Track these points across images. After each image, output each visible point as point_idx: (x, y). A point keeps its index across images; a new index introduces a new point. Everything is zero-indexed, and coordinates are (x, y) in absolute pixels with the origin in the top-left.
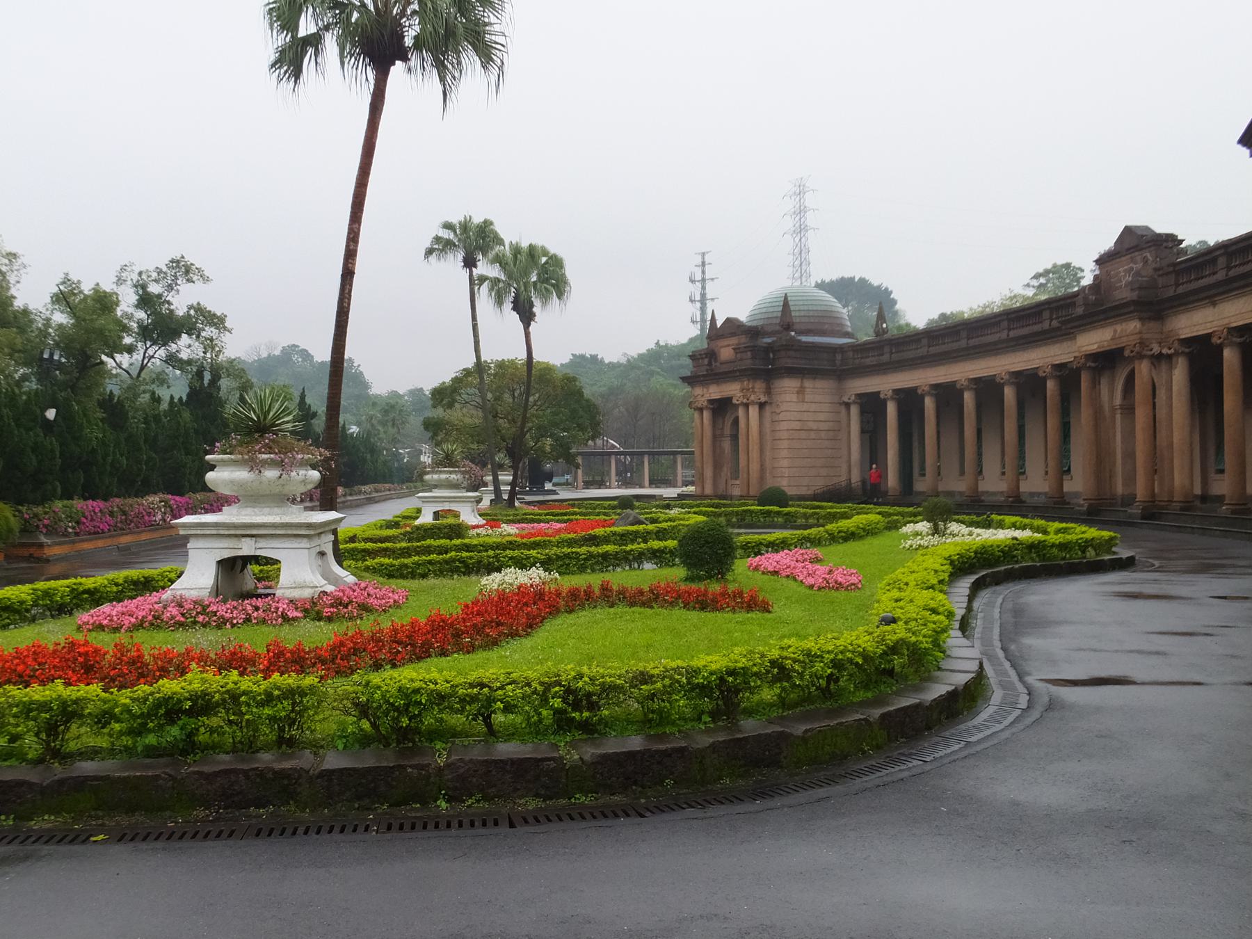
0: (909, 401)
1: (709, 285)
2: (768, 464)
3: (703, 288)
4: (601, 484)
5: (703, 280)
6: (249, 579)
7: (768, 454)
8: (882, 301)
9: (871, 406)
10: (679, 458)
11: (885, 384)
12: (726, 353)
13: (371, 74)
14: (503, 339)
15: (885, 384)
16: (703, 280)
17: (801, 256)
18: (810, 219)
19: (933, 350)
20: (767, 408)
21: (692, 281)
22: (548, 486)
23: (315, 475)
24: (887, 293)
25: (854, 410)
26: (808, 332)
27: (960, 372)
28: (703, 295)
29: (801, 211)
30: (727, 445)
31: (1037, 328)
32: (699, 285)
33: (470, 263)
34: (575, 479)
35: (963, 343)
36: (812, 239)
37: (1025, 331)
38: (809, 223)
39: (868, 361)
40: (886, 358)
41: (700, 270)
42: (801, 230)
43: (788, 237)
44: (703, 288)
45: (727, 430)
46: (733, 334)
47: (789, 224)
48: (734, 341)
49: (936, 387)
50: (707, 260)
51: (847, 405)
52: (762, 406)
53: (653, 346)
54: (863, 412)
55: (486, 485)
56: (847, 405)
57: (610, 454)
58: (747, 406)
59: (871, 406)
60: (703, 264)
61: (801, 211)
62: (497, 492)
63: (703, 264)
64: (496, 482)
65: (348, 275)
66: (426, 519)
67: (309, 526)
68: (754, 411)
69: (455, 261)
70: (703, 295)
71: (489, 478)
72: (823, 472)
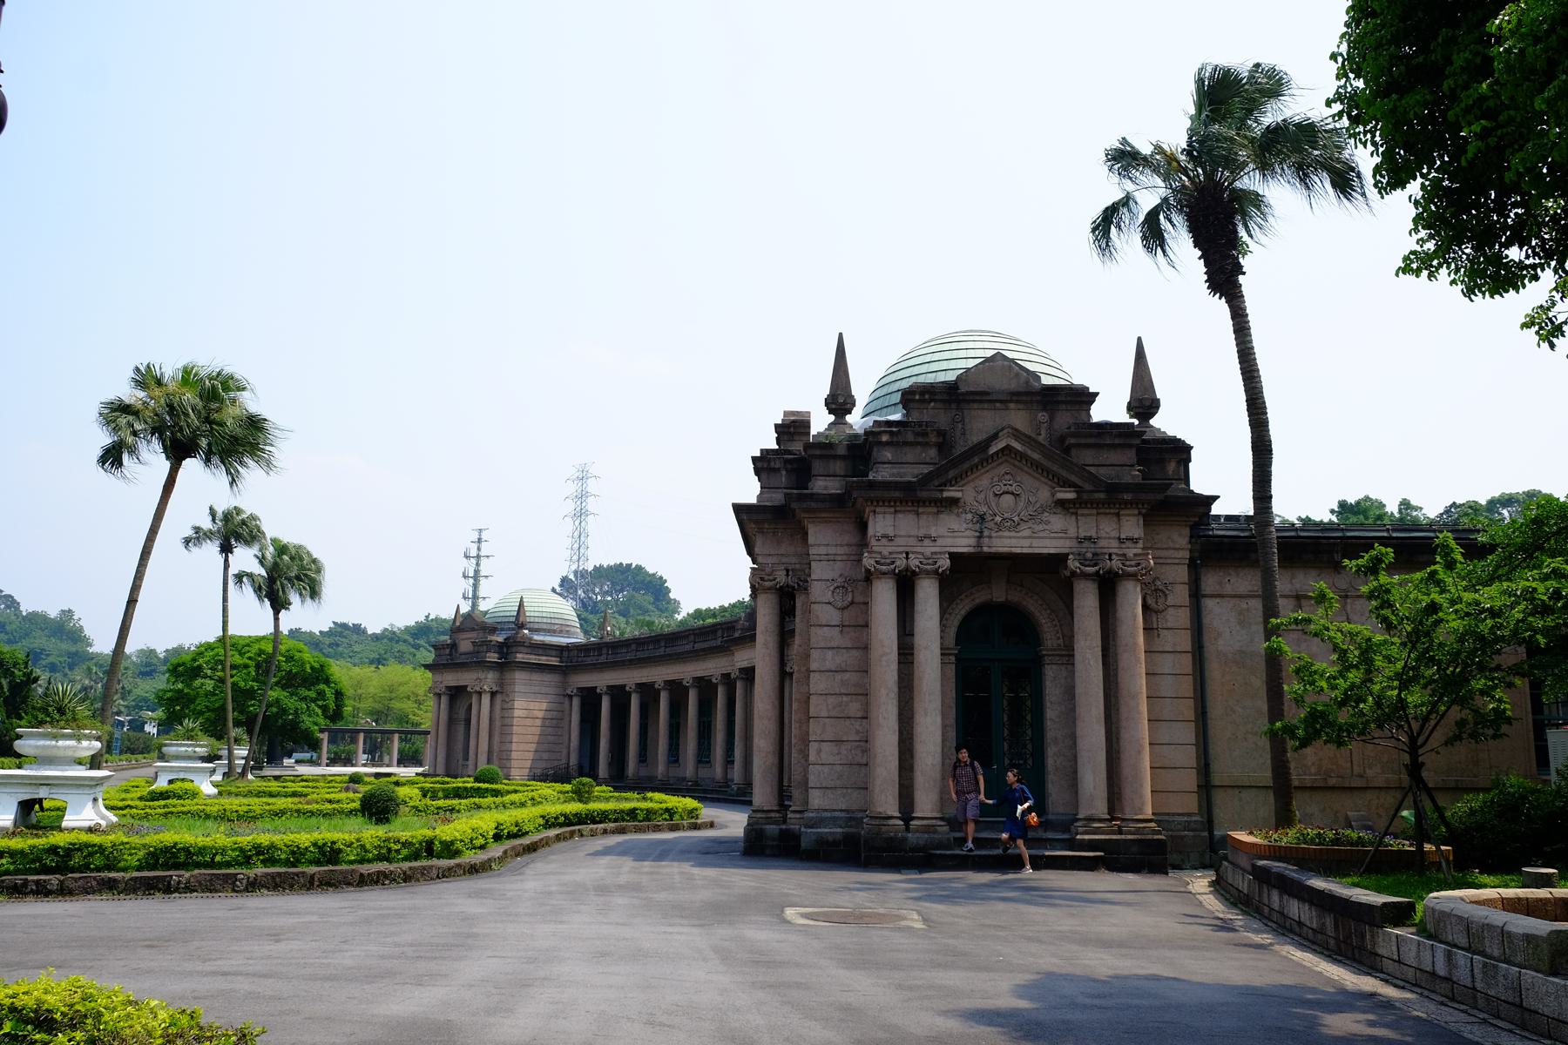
0: (619, 696)
1: (483, 562)
2: (496, 748)
3: (478, 564)
4: (348, 761)
5: (478, 557)
6: (36, 815)
7: (496, 739)
8: (655, 588)
9: (590, 699)
10: (362, 736)
11: (601, 680)
12: (465, 646)
13: (167, 465)
14: (252, 618)
15: (601, 680)
16: (478, 557)
17: (580, 540)
18: (591, 505)
19: (640, 655)
20: (499, 698)
21: (467, 557)
22: (286, 761)
23: (98, 745)
24: (662, 581)
25: (576, 702)
26: (537, 631)
27: (658, 675)
28: (477, 572)
29: (582, 496)
30: (461, 728)
31: (713, 644)
32: (474, 561)
33: (226, 549)
34: (319, 757)
35: (661, 651)
36: (591, 524)
37: (706, 645)
38: (589, 508)
39: (589, 660)
40: (602, 659)
41: (475, 546)
42: (581, 514)
43: (569, 520)
44: (478, 564)
45: (462, 714)
46: (473, 630)
47: (570, 506)
48: (473, 635)
49: (610, 688)
50: (484, 537)
51: (570, 697)
52: (493, 694)
53: (422, 619)
54: (583, 705)
55: (219, 758)
56: (570, 697)
57: (358, 731)
58: (480, 694)
59: (590, 699)
60: (480, 540)
61: (582, 496)
62: (231, 766)
63: (480, 540)
64: (230, 757)
65: (132, 602)
66: (162, 784)
67: (92, 778)
68: (486, 699)
69: (212, 549)
70: (477, 572)
71: (225, 753)
72: (545, 756)
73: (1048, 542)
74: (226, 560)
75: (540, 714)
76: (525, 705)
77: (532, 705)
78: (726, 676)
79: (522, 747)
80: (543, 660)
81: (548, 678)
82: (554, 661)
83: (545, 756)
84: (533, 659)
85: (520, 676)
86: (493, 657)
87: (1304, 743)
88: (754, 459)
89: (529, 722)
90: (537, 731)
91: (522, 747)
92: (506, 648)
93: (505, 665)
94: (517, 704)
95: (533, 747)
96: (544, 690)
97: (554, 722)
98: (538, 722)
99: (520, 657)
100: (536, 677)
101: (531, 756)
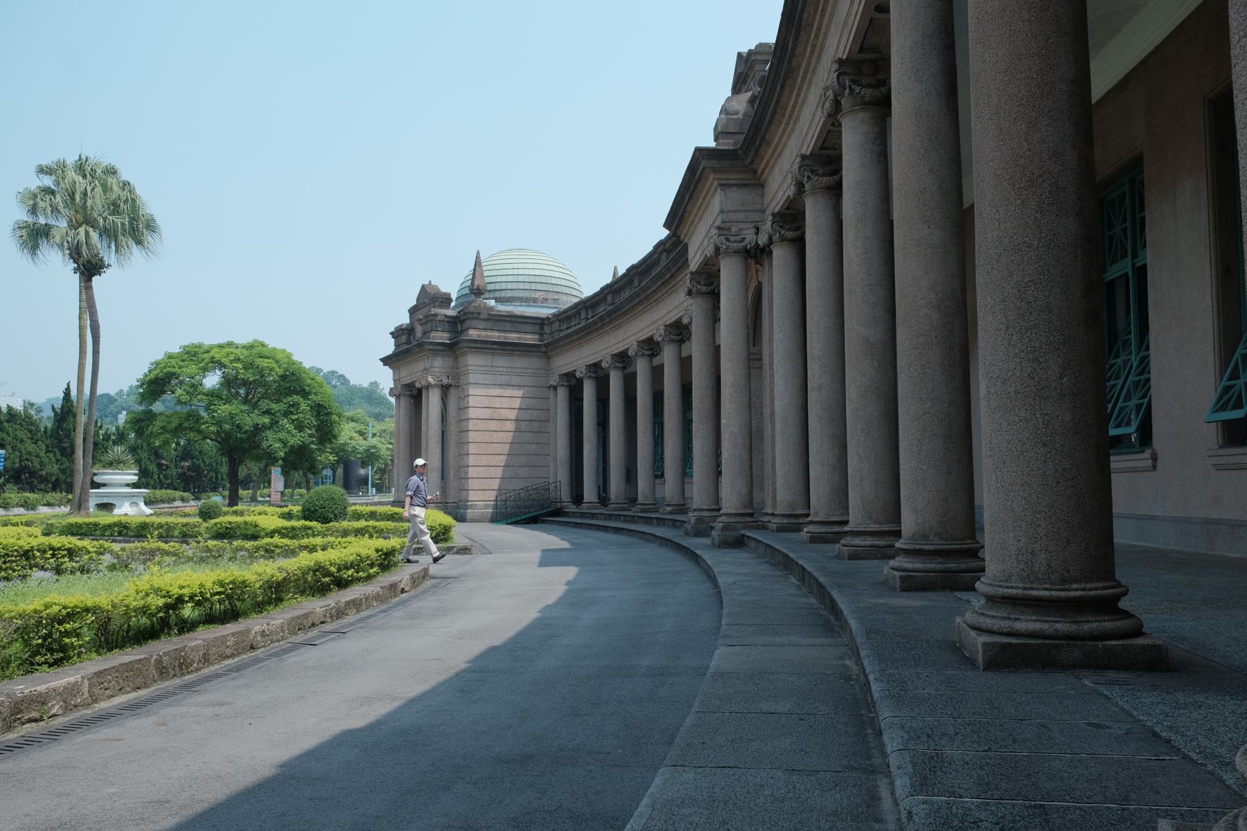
20: (453, 394)
51: (555, 388)
52: (445, 389)
56: (555, 388)
59: (574, 387)
72: (523, 472)
73: (528, 336)
74: (88, 305)
75: (512, 415)
76: (485, 402)
77: (497, 403)
78: (595, 367)
79: (484, 460)
80: (513, 337)
81: (520, 362)
82: (530, 339)
83: (523, 472)
84: (495, 336)
85: (474, 362)
86: (441, 337)
87: (115, 443)
88: (740, 55)
89: (493, 425)
90: (508, 437)
91: (484, 460)
92: (457, 324)
93: (452, 349)
94: (472, 401)
95: (501, 460)
96: (515, 380)
97: (531, 426)
98: (510, 426)
99: (473, 334)
100: (502, 362)
101: (499, 472)
